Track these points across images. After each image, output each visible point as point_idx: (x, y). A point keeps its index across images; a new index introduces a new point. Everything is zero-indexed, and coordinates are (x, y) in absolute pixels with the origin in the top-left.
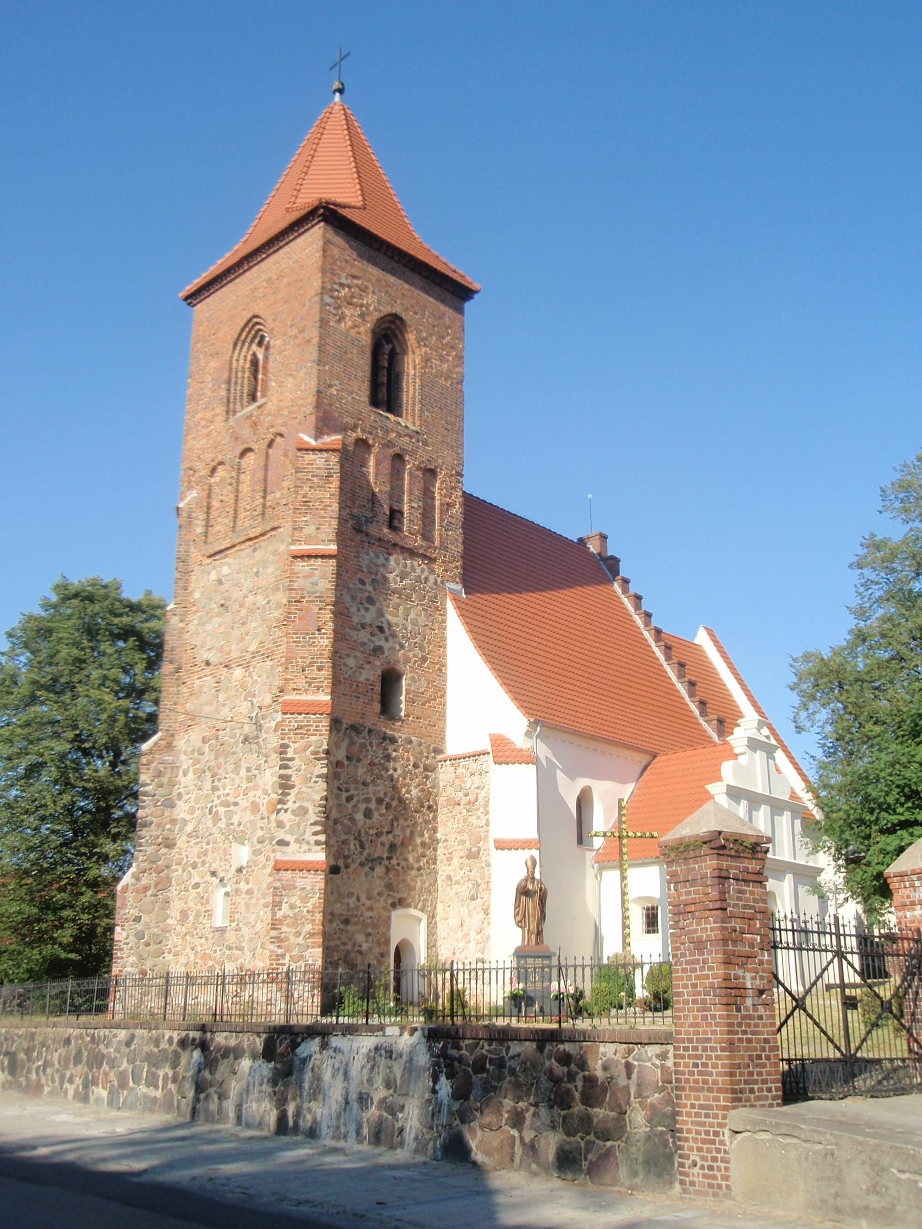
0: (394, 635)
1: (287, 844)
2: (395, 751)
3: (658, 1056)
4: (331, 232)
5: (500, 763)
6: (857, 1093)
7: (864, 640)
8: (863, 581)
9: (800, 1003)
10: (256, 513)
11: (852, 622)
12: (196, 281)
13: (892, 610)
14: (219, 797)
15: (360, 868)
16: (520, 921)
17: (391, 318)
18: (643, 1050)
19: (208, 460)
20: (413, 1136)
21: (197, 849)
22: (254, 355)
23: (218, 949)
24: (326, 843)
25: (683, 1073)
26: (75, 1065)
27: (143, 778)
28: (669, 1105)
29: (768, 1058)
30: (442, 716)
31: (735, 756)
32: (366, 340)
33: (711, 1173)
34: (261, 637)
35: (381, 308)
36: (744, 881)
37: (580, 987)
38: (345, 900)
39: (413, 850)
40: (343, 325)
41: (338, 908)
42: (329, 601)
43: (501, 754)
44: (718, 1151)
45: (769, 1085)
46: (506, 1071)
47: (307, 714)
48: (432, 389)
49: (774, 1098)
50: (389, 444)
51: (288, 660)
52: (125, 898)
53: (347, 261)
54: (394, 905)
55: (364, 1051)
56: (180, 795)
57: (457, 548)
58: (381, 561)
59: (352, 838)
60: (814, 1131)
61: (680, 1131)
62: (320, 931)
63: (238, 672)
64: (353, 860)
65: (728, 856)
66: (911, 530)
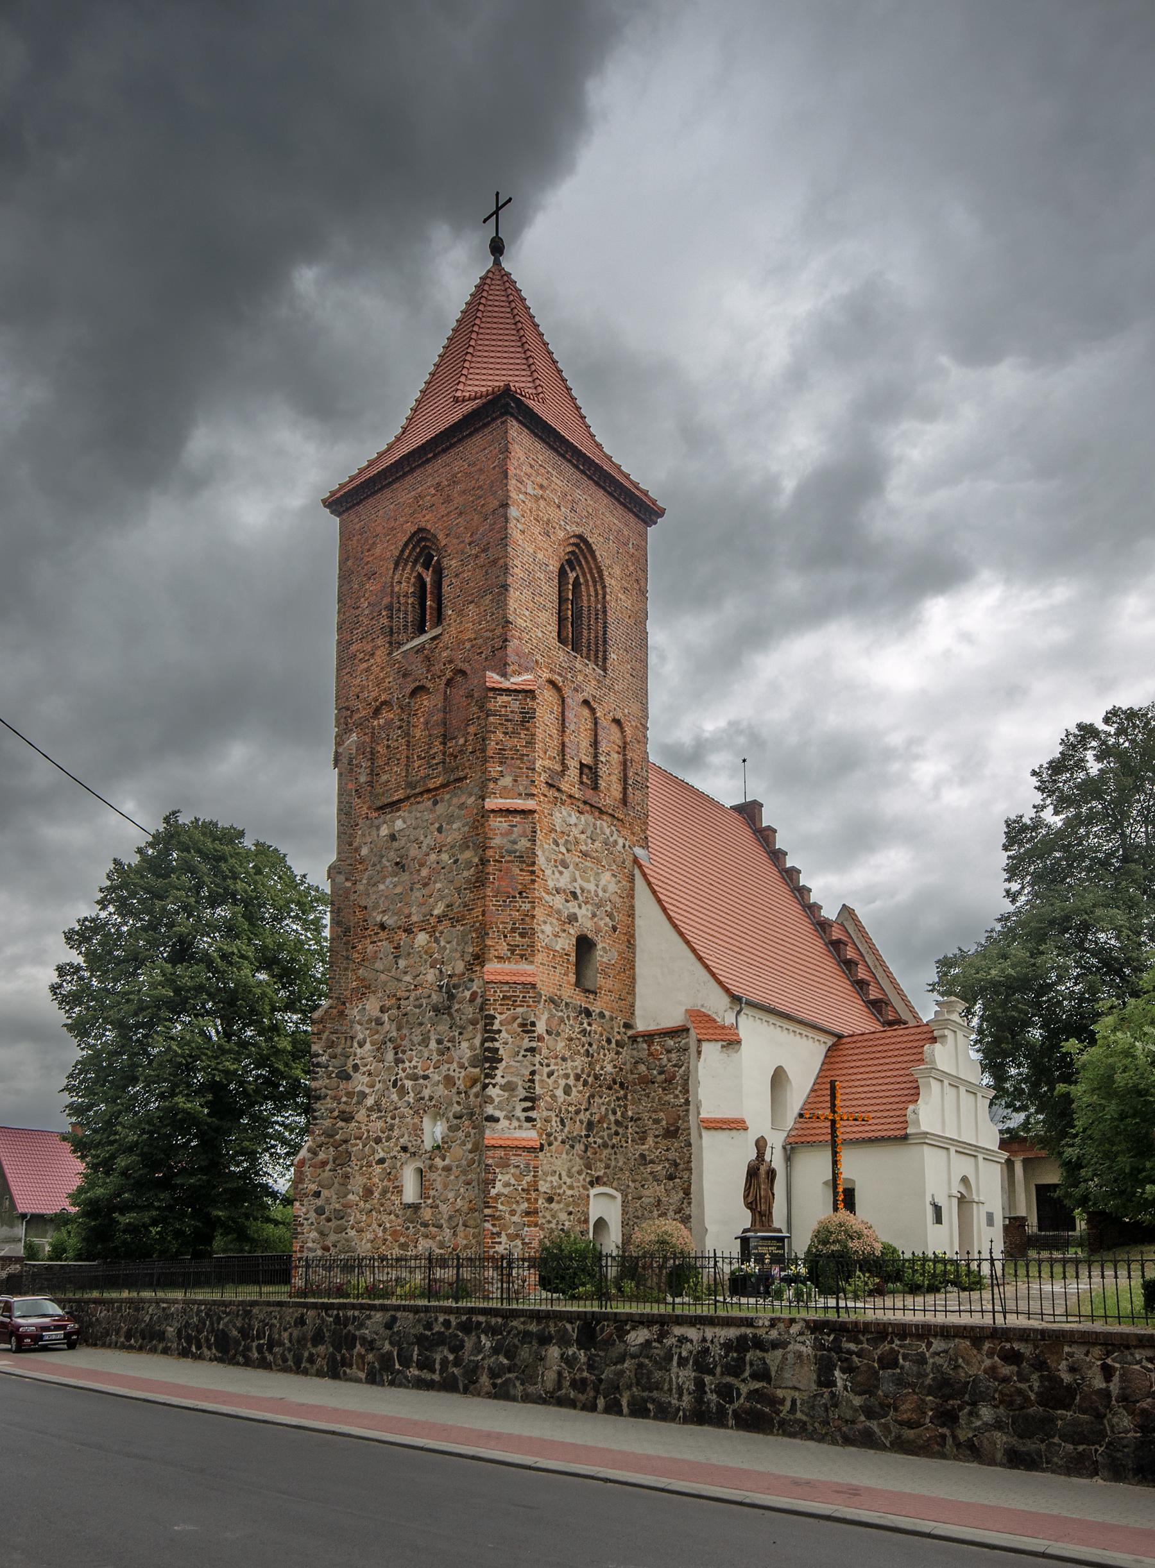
1: (497, 1120)
14: (404, 1070)
16: (751, 1203)
21: (380, 1124)
22: (420, 578)
23: (411, 1226)
32: (554, 567)
56: (356, 1068)
63: (422, 938)
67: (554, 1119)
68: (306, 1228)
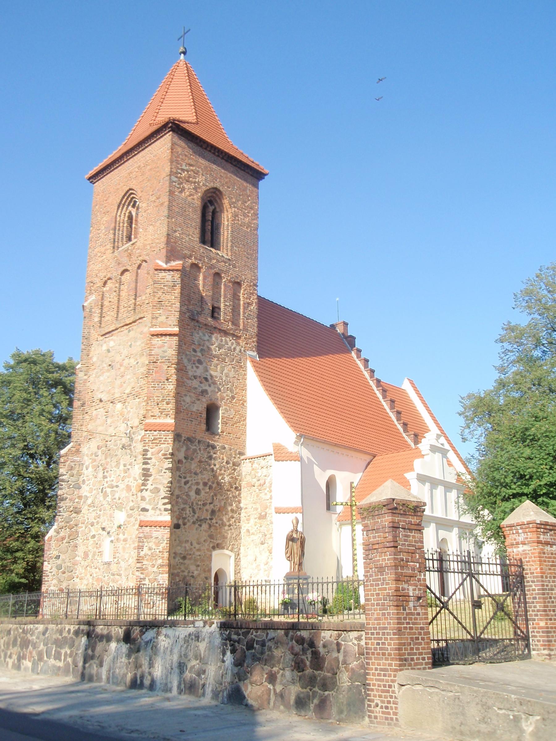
0: (214, 383)
1: (147, 510)
2: (215, 453)
3: (356, 638)
4: (176, 137)
5: (279, 461)
6: (484, 661)
7: (504, 386)
8: (503, 350)
9: (445, 605)
10: (130, 309)
11: (496, 375)
12: (95, 168)
13: (522, 368)
14: (107, 482)
15: (193, 525)
16: (289, 557)
17: (215, 190)
18: (347, 635)
19: (102, 277)
20: (210, 689)
21: (94, 514)
22: (130, 212)
23: (106, 575)
24: (171, 510)
25: (371, 649)
26: (13, 647)
27: (62, 471)
28: (362, 669)
29: (423, 639)
30: (244, 432)
31: (423, 456)
32: (198, 203)
33: (387, 711)
34: (132, 385)
35: (207, 184)
36: (409, 529)
37: (325, 595)
38: (183, 545)
39: (226, 514)
40: (183, 194)
41: (179, 550)
42: (173, 362)
43: (279, 455)
44: (391, 697)
45: (424, 656)
46: (266, 648)
47: (160, 431)
48: (238, 233)
49: (426, 664)
50: (212, 267)
51: (149, 398)
52: (50, 544)
53: (186, 156)
54: (214, 548)
55: (182, 636)
57: (253, 330)
58: (206, 338)
59: (188, 506)
60: (448, 684)
61: (369, 685)
62: (167, 564)
63: (119, 406)
64: (188, 520)
65: (399, 514)
66: (532, 319)
67: (188, 509)
68: (50, 577)
